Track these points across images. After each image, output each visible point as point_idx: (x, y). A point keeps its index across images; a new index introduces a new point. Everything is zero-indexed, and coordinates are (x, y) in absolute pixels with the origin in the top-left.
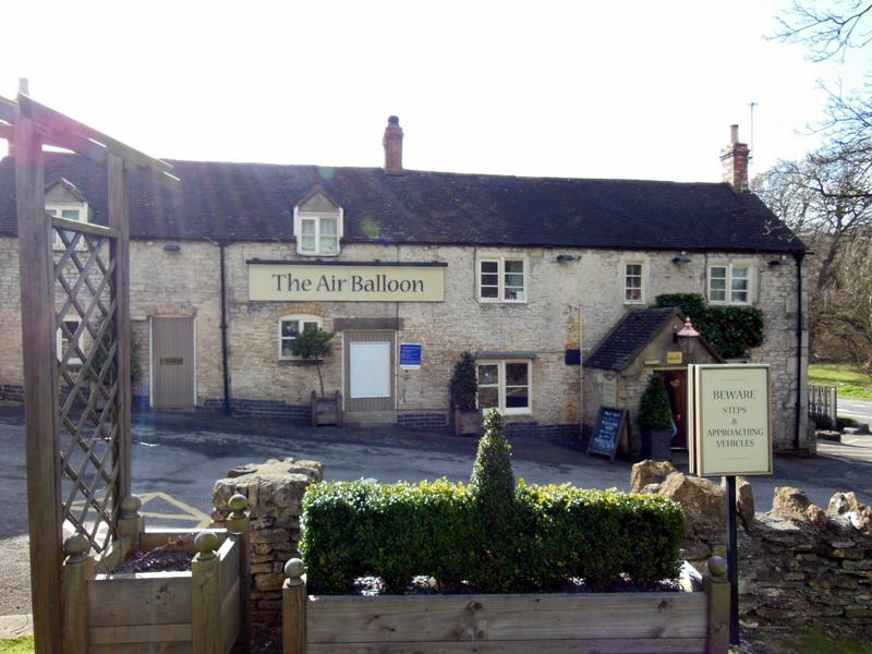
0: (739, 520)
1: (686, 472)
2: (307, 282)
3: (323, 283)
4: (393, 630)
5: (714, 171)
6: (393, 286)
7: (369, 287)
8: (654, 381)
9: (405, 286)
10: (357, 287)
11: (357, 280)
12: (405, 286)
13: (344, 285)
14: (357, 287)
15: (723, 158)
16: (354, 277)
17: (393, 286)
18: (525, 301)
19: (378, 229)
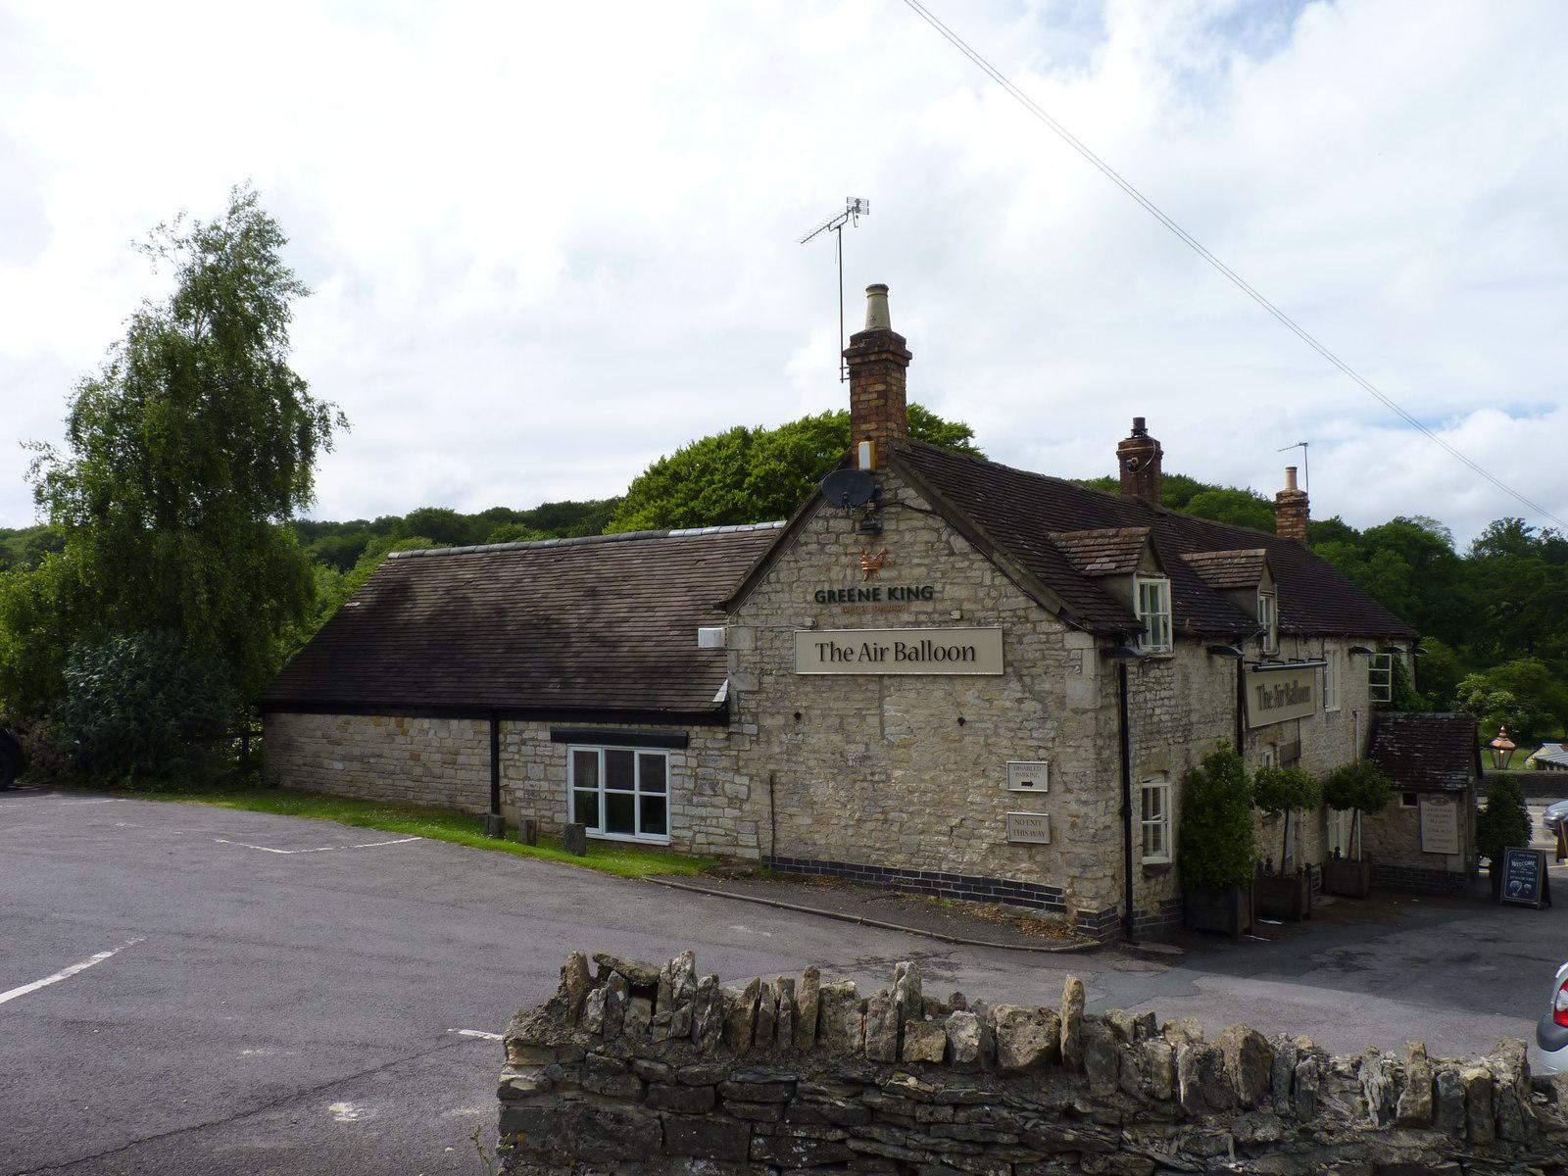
0: (955, 581)
1: (1261, 647)
2: (849, 652)
3: (865, 652)
4: (856, 208)
5: (1269, 488)
6: (940, 654)
7: (913, 656)
8: (1189, 806)
9: (954, 654)
10: (901, 656)
11: (900, 647)
12: (954, 654)
13: (886, 656)
14: (901, 656)
15: (1474, 541)
16: (896, 644)
17: (940, 654)
18: (1339, 709)
19: (312, 467)
